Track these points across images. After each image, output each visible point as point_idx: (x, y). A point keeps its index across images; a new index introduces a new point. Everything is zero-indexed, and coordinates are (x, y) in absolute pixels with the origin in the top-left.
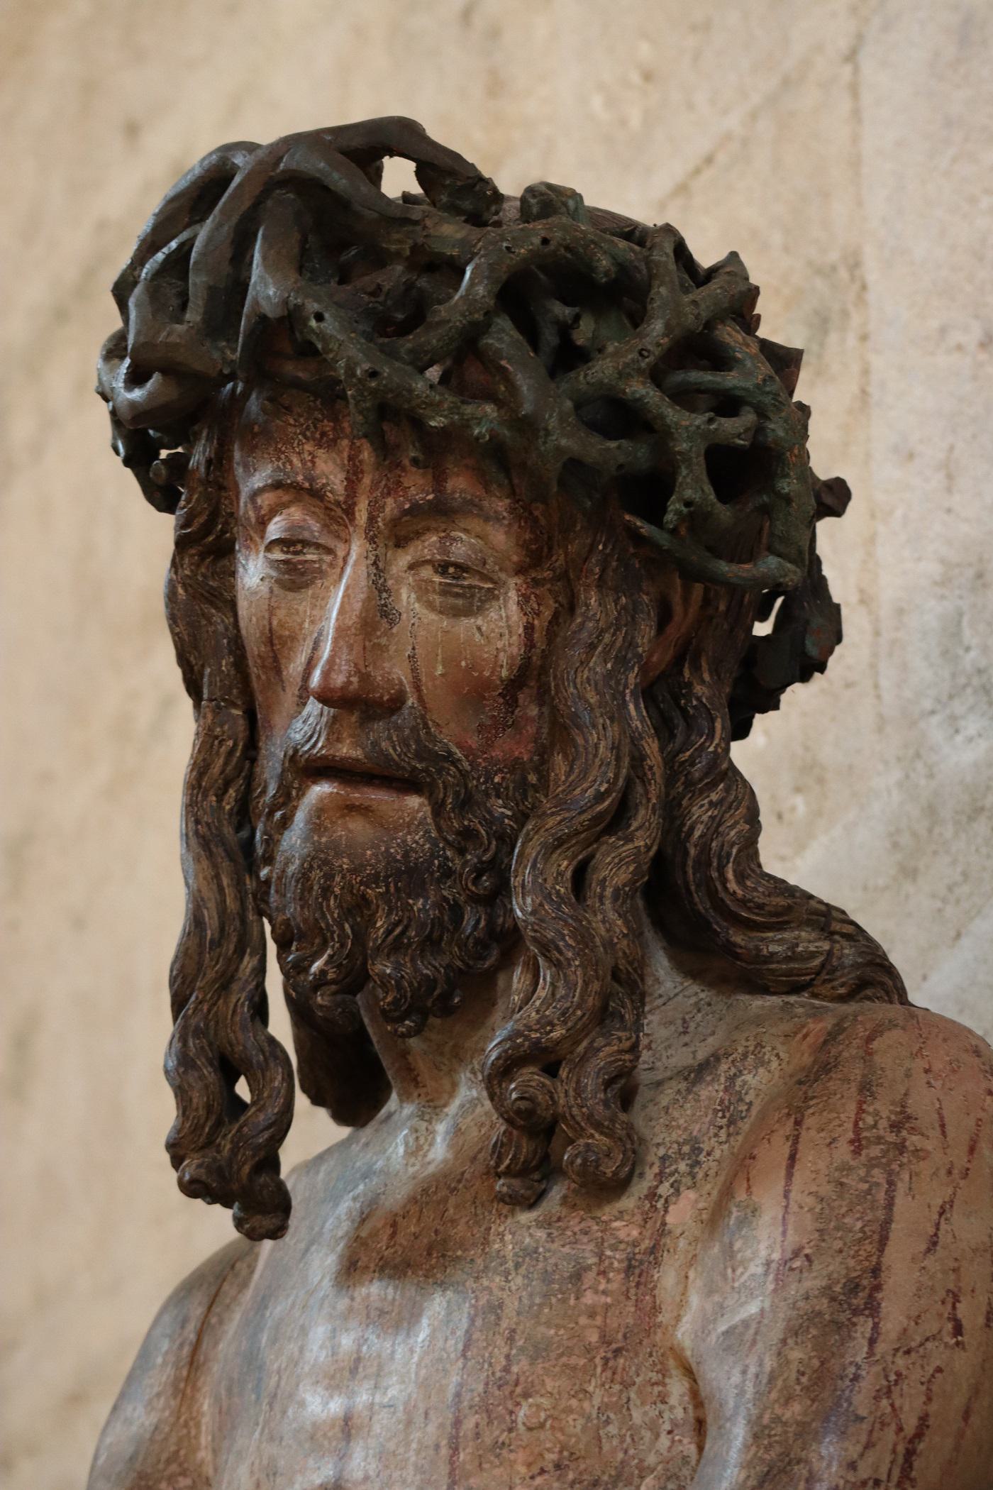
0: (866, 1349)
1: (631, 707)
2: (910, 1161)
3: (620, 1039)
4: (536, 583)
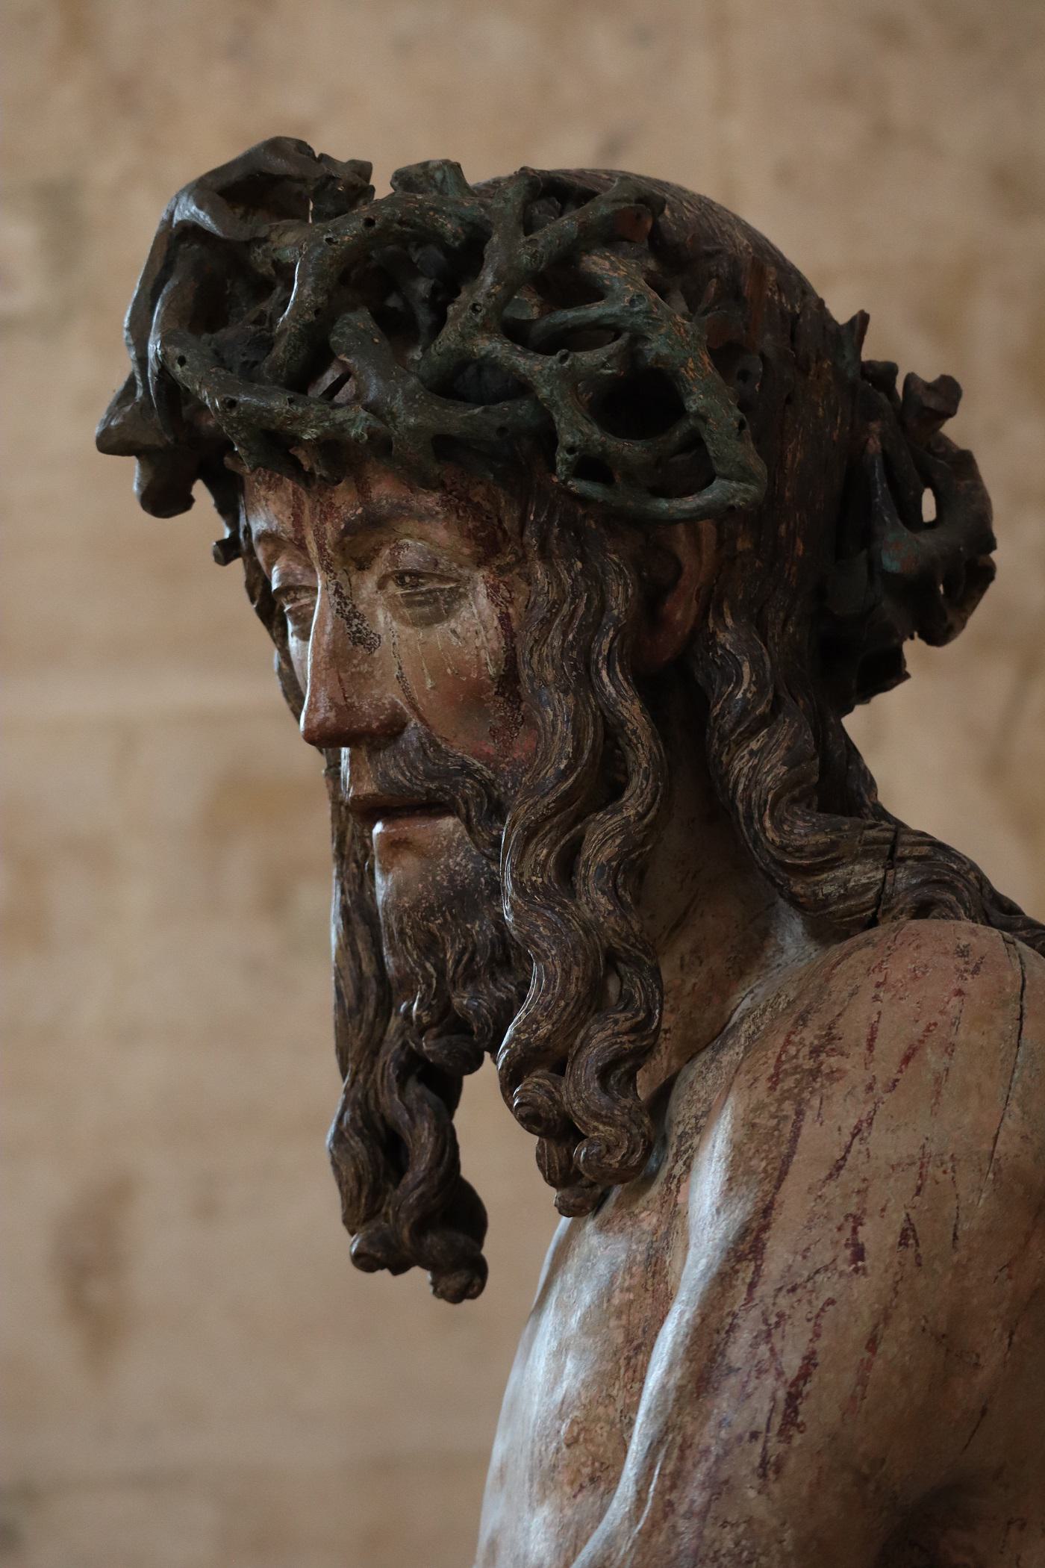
0: (744, 1296)
1: (604, 673)
2: (822, 1086)
3: (616, 1022)
4: (502, 570)
